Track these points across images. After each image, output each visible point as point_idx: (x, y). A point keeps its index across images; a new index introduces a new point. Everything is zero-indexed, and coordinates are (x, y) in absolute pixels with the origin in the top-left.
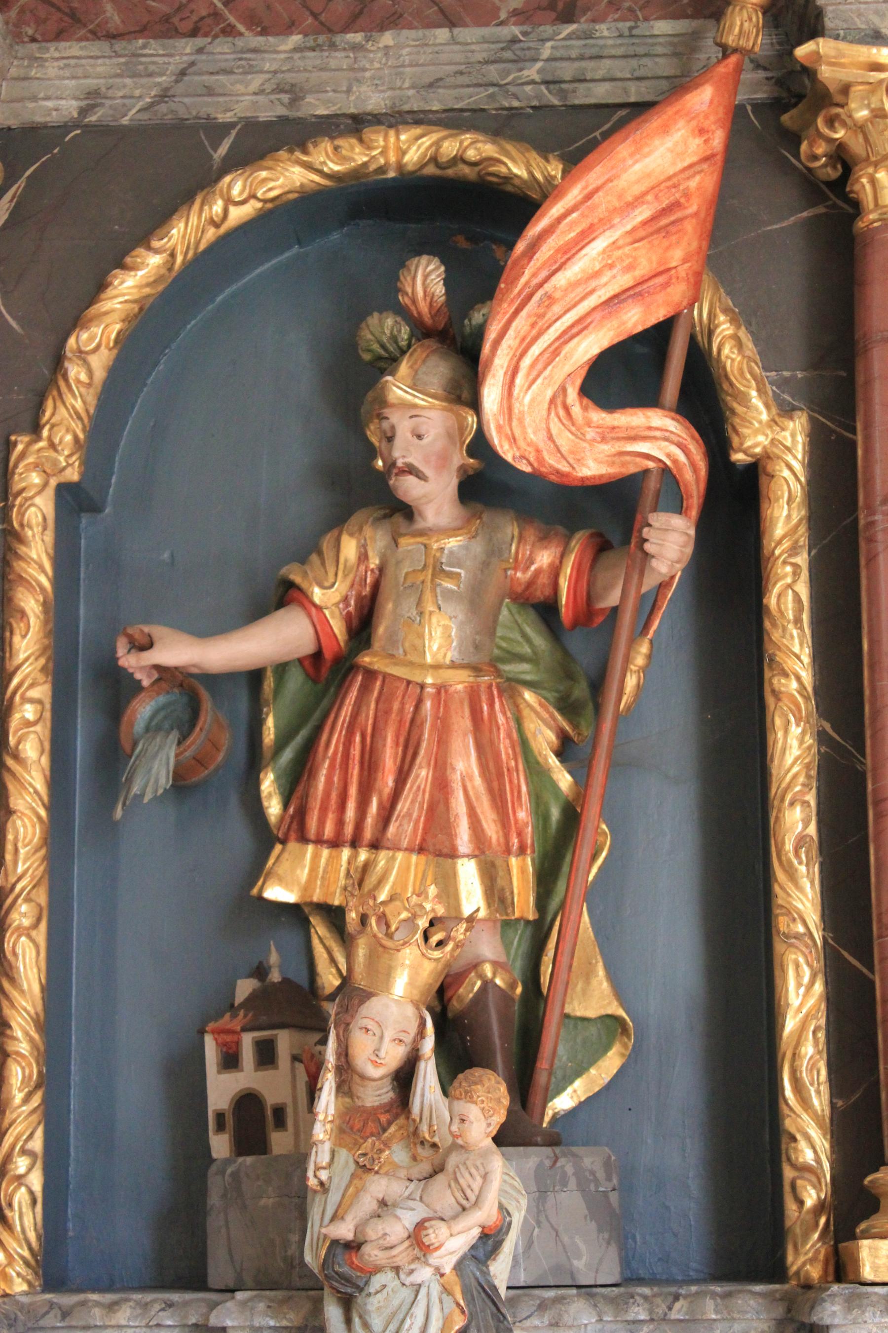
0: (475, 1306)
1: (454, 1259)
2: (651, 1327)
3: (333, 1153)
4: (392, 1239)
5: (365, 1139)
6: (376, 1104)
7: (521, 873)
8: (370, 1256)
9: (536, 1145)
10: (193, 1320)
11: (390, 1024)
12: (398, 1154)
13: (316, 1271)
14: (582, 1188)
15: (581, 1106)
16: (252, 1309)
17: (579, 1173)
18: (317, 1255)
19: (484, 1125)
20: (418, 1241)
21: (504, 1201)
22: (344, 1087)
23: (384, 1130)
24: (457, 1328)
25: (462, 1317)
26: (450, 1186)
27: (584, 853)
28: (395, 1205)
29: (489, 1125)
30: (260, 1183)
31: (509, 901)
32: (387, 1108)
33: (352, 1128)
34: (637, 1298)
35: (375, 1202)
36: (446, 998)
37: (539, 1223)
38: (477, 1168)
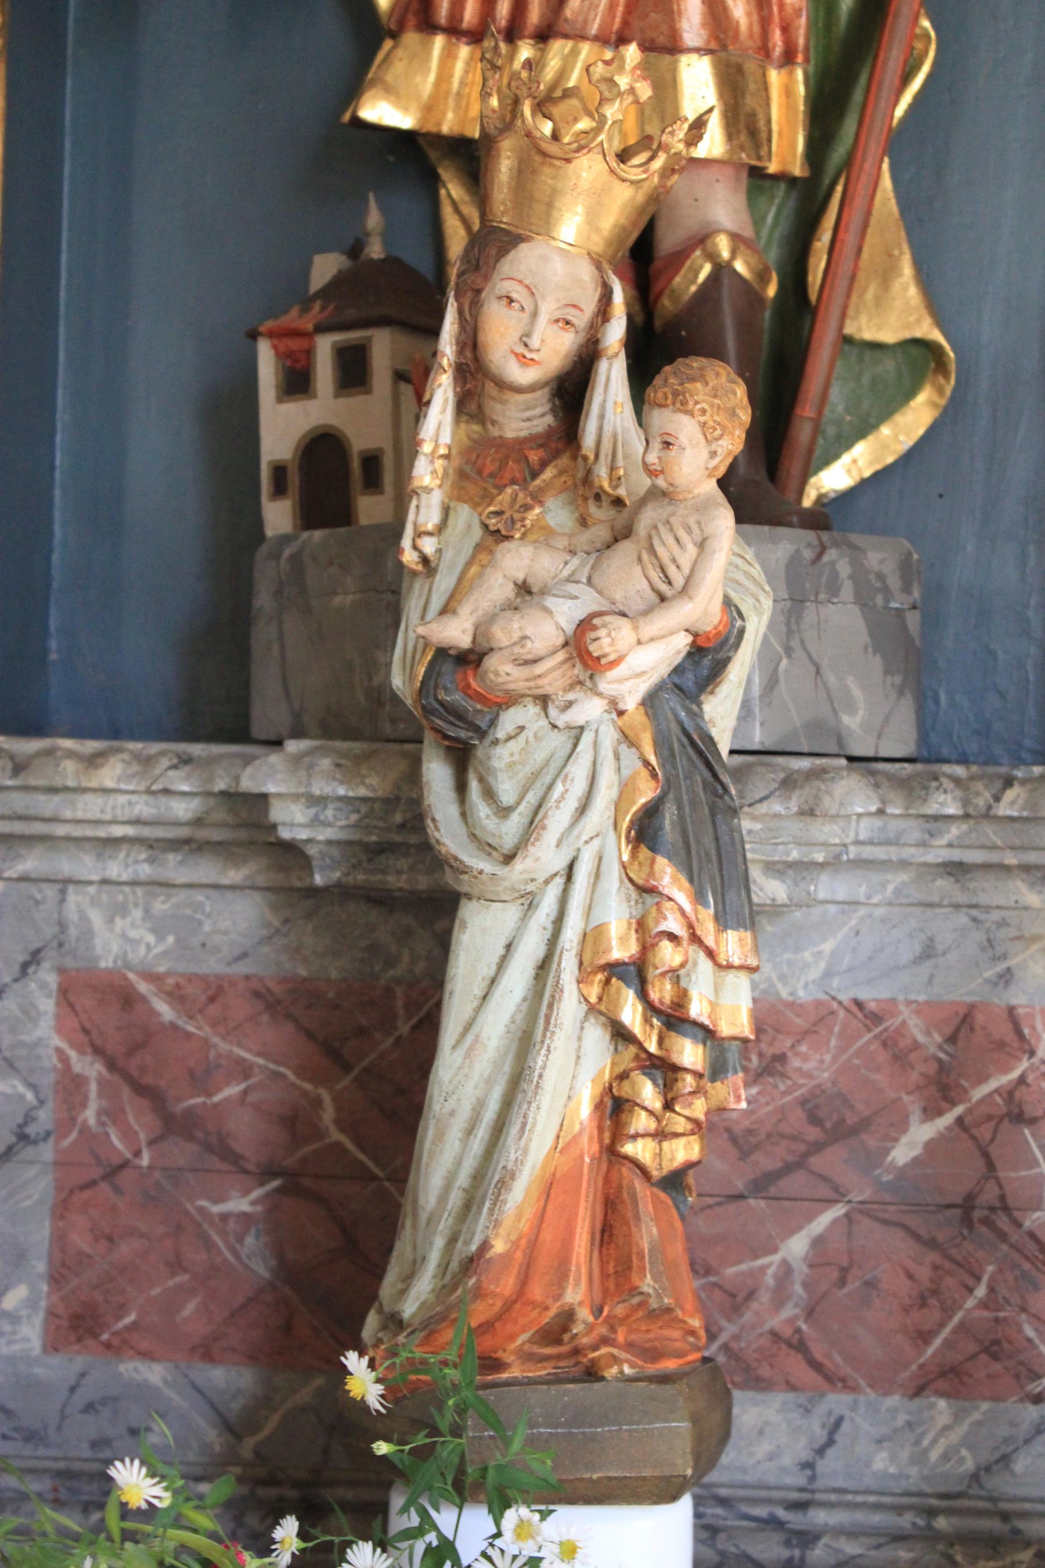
0: (675, 768)
1: (643, 687)
2: (964, 827)
3: (446, 511)
4: (537, 646)
5: (501, 488)
6: (524, 434)
7: (785, 95)
8: (497, 674)
9: (790, 525)
10: (220, 785)
11: (548, 295)
12: (556, 513)
13: (409, 702)
14: (863, 600)
15: (864, 484)
16: (311, 767)
17: (859, 575)
18: (412, 677)
19: (705, 455)
20: (581, 651)
21: (732, 594)
22: (469, 405)
23: (535, 475)
24: (642, 800)
25: (653, 784)
26: (640, 560)
27: (892, 59)
28: (544, 592)
29: (713, 454)
30: (334, 570)
31: (764, 136)
32: (541, 441)
33: (480, 473)
34: (944, 780)
35: (511, 586)
36: (652, 297)
37: (789, 651)
38: (689, 530)
